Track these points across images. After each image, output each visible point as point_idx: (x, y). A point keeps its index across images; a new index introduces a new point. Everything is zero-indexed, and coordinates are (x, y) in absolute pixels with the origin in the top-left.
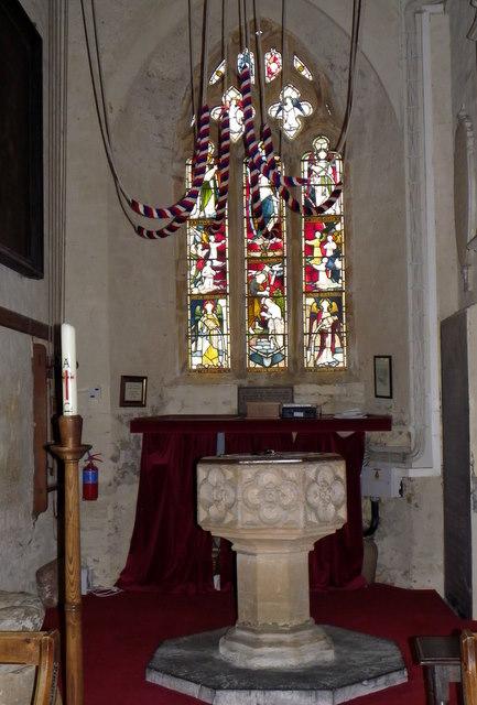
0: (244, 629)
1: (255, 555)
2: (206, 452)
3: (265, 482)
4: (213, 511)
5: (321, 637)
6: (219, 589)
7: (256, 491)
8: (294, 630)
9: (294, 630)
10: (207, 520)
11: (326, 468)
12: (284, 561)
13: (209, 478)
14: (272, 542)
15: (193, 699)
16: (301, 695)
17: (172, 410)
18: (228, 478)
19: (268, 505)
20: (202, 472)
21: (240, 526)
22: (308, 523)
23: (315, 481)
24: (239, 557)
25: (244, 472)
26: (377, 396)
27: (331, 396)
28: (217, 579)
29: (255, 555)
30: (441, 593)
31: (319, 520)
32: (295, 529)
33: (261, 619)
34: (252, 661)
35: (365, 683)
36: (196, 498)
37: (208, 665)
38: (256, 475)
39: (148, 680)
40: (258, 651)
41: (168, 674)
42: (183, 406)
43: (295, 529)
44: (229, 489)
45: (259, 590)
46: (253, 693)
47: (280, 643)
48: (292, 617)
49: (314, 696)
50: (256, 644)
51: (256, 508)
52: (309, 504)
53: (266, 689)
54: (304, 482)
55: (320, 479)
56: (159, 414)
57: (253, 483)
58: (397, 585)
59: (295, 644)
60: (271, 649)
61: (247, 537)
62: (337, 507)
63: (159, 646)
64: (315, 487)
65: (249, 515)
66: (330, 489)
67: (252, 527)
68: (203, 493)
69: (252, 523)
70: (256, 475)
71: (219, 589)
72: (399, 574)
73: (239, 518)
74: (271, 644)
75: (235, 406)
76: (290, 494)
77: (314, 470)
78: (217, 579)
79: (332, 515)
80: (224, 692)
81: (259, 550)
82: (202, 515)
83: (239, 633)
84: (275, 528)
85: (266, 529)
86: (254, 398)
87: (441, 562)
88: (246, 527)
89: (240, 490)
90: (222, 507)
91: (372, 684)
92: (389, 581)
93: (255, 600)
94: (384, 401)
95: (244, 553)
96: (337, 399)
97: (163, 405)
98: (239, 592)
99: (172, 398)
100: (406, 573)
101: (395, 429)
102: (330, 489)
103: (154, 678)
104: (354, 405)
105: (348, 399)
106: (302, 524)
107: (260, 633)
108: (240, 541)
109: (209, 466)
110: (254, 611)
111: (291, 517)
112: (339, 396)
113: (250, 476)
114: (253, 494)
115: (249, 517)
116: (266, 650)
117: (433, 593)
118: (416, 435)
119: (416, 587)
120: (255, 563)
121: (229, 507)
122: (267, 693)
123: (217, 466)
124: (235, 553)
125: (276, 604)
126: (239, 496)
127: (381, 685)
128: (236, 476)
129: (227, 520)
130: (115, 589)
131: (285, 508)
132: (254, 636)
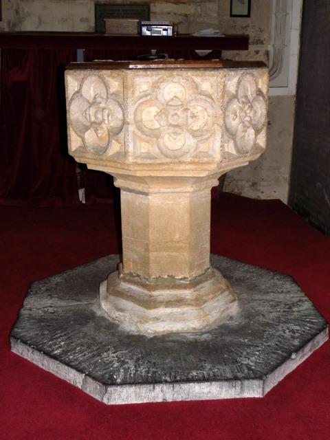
0: (125, 280)
1: (147, 194)
2: (70, 63)
3: (168, 97)
4: (90, 136)
5: (223, 286)
6: (84, 202)
7: (154, 110)
8: (195, 283)
9: (195, 283)
10: (84, 147)
11: (249, 78)
12: (184, 202)
13: (85, 90)
14: (172, 180)
15: (76, 389)
16: (221, 387)
17: (29, 26)
18: (112, 90)
19: (171, 130)
20: (72, 81)
21: (131, 160)
22: (225, 156)
23: (235, 96)
24: (124, 196)
25: (138, 80)
26: (232, 16)
27: (186, 16)
28: (81, 192)
29: (147, 194)
30: (285, 201)
31: (238, 151)
32: (209, 163)
33: (154, 272)
34: (147, 326)
35: (293, 356)
36: (254, 200)
37: (88, 329)
38: (156, 86)
39: (14, 351)
40: (153, 313)
41: (40, 350)
42: (40, 22)
43: (209, 163)
44: (113, 106)
45: (152, 236)
46: (158, 388)
47: (179, 302)
48: (191, 269)
49: (238, 389)
50: (149, 303)
51: (155, 135)
52: (227, 129)
53: (175, 381)
54: (223, 96)
55: (240, 94)
56: (17, 29)
57: (149, 98)
58: (243, 195)
59: (198, 302)
60: (168, 310)
61: (138, 174)
62: (257, 132)
63: (26, 296)
64: (235, 105)
65: (143, 144)
66: (251, 107)
67: (148, 161)
68: (75, 112)
69: (148, 156)
70: (156, 86)
71: (84, 202)
72: (247, 185)
73: (131, 148)
74: (169, 304)
75: (92, 23)
76: (204, 114)
77: (236, 80)
78: (81, 192)
79: (252, 143)
80: (119, 388)
81: (154, 188)
82: (74, 143)
83: (125, 286)
84: (180, 162)
85: (167, 164)
86: (112, 16)
87: (287, 176)
88: (139, 161)
89: (131, 110)
90: (103, 133)
91: (300, 354)
92: (236, 190)
93: (147, 250)
94: (240, 21)
95: (131, 191)
96: (192, 19)
97: (20, 21)
98: (124, 237)
99: (29, 14)
100: (254, 184)
101: (252, 48)
102: (251, 107)
103: (19, 349)
104: (208, 26)
105: (202, 19)
106: (218, 157)
107: (156, 288)
108: (125, 177)
109: (82, 73)
110: (145, 262)
111: (203, 147)
112: (194, 16)
113: (145, 87)
114: (149, 115)
115: (144, 148)
116: (162, 311)
117: (278, 202)
118: (275, 55)
119: (263, 197)
120: (148, 205)
121: (115, 133)
122: (177, 387)
123: (96, 72)
124: (118, 191)
125: (174, 254)
126: (130, 118)
127: (307, 353)
128: (124, 86)
129: (111, 152)
130: (105, 20)
131: (194, 134)
132: (146, 292)
